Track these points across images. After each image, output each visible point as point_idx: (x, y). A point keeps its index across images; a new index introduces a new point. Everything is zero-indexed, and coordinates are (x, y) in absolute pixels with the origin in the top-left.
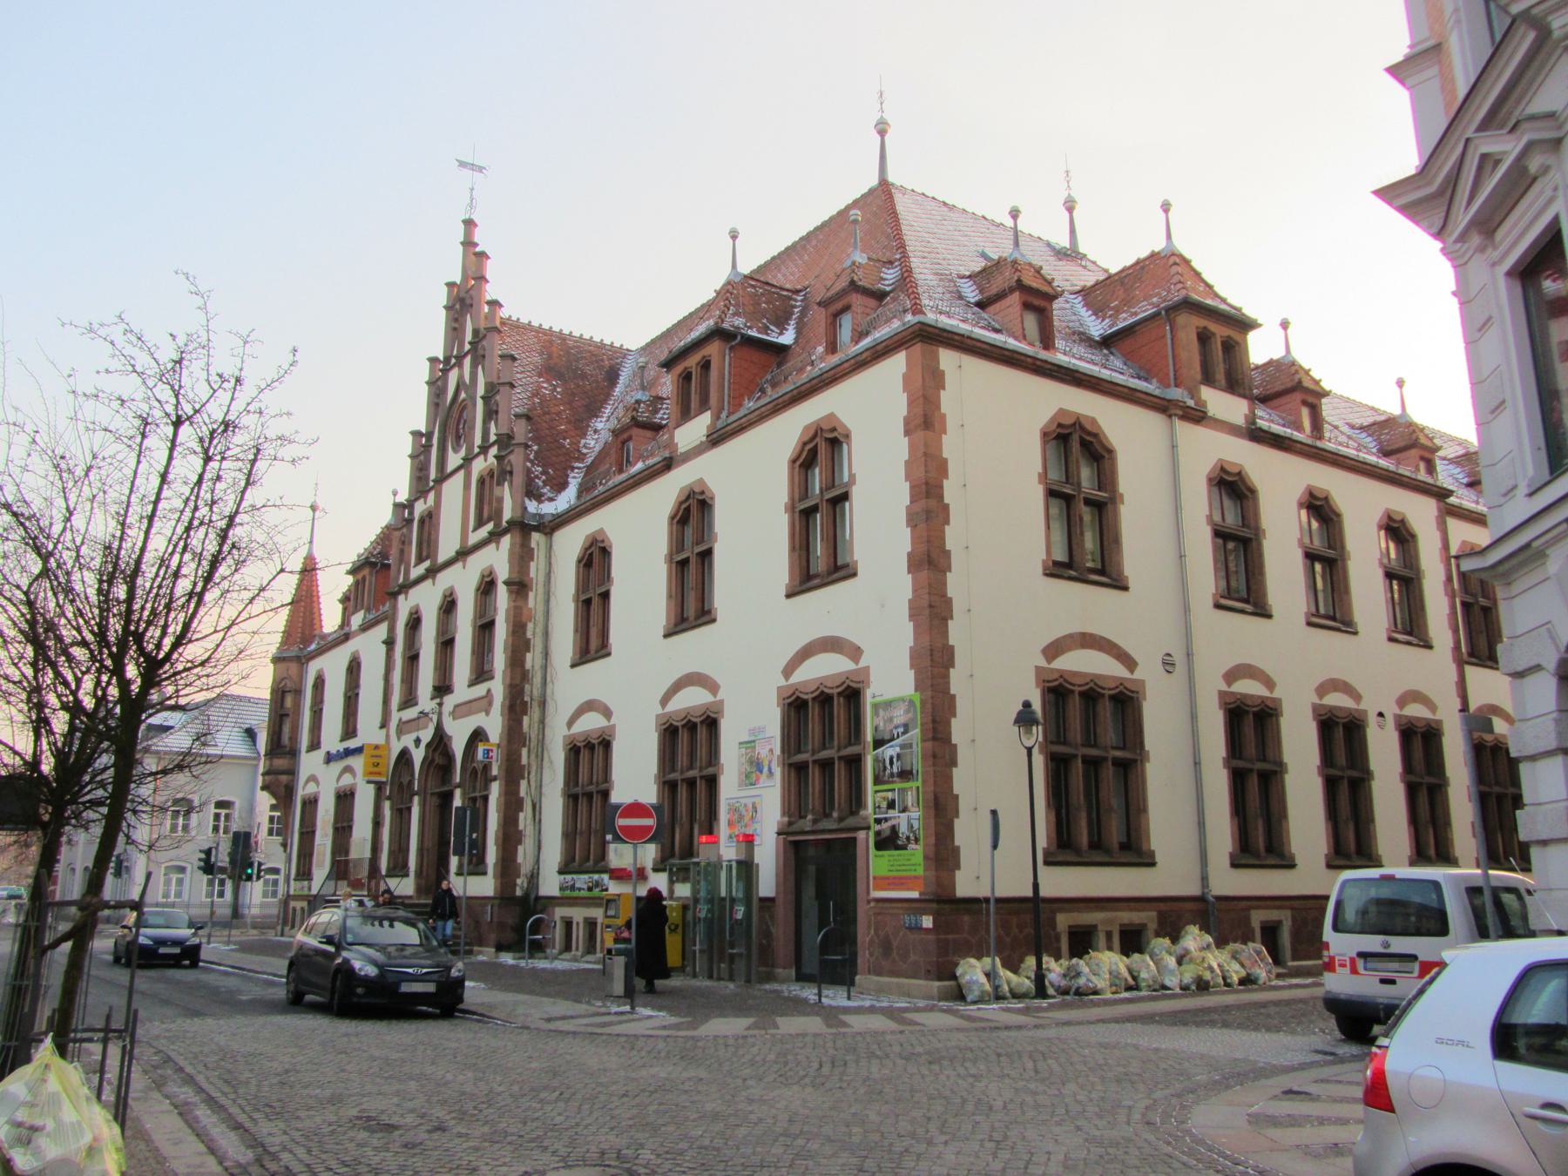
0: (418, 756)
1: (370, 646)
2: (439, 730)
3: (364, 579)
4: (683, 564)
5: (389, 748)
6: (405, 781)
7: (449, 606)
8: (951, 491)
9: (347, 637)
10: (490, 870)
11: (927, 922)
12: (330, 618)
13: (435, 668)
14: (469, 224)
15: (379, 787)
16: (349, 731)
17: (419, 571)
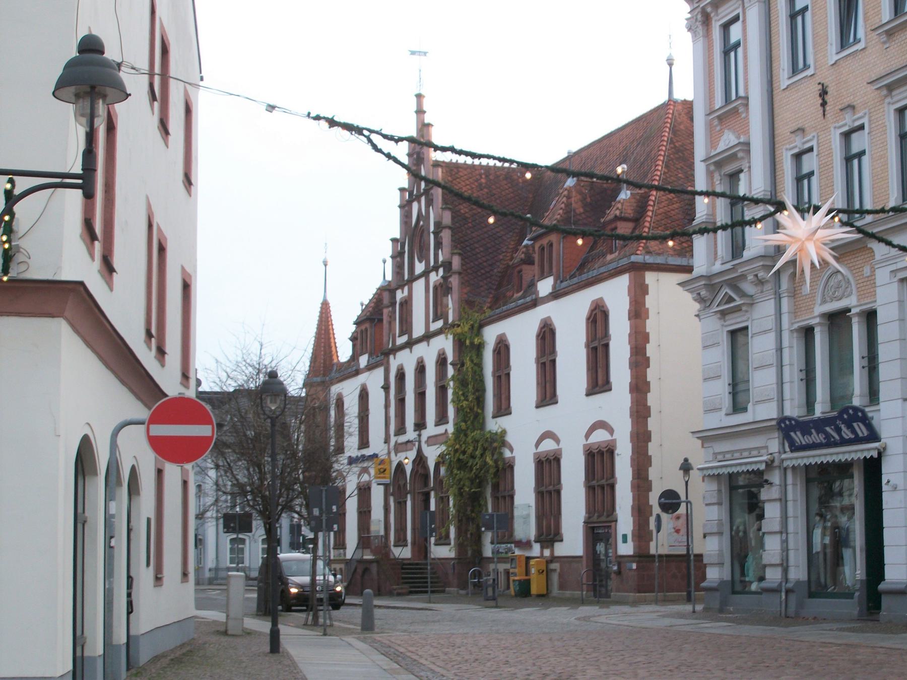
0: (408, 469)
1: (374, 380)
2: (420, 451)
3: (366, 330)
4: (544, 364)
5: (391, 462)
6: (402, 483)
7: (421, 369)
8: (651, 350)
9: (357, 372)
10: (452, 542)
11: (634, 566)
12: (344, 351)
13: (415, 411)
14: (419, 97)
15: (386, 486)
16: (364, 443)
17: (401, 340)
